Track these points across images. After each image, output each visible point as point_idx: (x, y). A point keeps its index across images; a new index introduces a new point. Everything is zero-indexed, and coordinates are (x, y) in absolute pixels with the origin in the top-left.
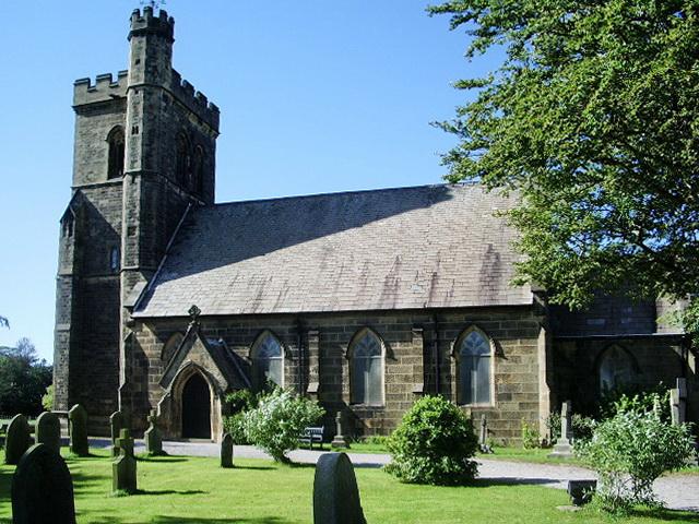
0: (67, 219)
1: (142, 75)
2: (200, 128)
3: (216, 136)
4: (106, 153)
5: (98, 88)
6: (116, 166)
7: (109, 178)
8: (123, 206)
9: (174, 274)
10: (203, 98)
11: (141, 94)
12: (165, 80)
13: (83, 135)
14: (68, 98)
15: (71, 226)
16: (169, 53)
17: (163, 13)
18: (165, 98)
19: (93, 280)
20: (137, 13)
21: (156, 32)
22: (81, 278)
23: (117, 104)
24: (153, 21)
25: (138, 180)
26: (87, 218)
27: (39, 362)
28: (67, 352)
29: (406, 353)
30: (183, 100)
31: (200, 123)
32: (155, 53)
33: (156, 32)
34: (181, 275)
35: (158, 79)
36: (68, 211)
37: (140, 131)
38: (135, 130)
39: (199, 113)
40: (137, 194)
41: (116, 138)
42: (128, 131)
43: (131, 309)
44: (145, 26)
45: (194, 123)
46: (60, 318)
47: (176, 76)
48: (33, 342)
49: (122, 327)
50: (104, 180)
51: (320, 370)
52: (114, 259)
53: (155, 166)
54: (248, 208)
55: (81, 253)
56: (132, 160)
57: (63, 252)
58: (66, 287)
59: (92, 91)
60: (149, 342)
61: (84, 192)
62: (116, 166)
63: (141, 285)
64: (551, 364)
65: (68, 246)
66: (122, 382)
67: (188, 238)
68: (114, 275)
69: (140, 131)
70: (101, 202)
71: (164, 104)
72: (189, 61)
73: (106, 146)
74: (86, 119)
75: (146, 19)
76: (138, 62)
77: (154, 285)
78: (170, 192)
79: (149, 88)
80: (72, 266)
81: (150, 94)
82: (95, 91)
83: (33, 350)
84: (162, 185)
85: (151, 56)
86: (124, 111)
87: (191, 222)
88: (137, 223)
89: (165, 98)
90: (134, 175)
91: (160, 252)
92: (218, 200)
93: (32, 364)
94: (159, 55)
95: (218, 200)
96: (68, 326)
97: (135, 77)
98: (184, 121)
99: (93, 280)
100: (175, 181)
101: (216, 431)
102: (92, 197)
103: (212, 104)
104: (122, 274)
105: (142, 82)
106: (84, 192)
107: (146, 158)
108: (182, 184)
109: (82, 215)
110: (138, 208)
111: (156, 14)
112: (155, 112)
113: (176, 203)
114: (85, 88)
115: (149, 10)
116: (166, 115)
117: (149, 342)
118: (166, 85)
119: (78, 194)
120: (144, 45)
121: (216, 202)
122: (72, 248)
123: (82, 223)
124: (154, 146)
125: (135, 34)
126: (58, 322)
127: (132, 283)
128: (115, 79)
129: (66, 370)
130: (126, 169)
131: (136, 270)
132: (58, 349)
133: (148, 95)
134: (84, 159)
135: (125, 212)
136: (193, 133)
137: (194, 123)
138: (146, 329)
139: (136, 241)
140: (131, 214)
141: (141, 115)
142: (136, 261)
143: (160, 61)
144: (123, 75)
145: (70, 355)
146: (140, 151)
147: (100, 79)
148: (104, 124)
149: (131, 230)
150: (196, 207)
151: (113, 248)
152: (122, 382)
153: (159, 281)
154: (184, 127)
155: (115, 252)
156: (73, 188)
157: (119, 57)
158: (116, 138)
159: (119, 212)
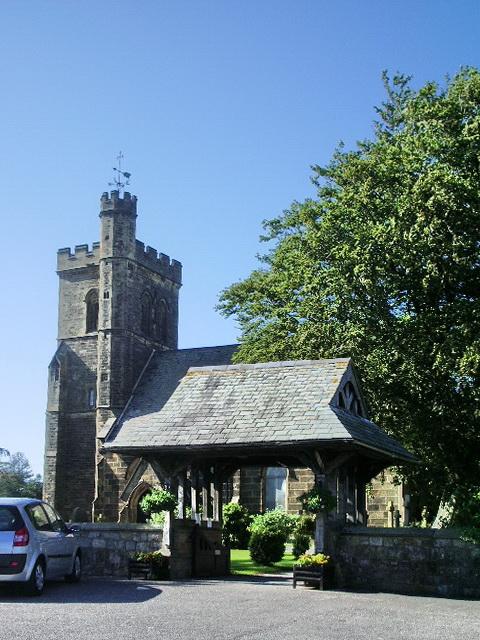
0: (54, 364)
1: (111, 249)
2: (163, 284)
3: (179, 288)
4: (85, 311)
5: (77, 256)
6: (92, 324)
7: (87, 332)
8: (98, 355)
9: (138, 411)
10: (165, 258)
11: (110, 265)
12: (130, 251)
13: (65, 295)
14: (52, 264)
15: (57, 371)
16: (132, 228)
17: (127, 194)
18: (131, 267)
19: (74, 416)
20: (105, 195)
21: (121, 210)
22: (65, 413)
23: (91, 271)
24: (119, 203)
25: (109, 336)
26: (70, 365)
27: (33, 478)
28: (53, 473)
29: (303, 473)
30: (146, 265)
31: (163, 279)
32: (121, 229)
33: (121, 210)
34: (144, 412)
35: (124, 251)
36: (55, 358)
37: (111, 295)
38: (106, 295)
39: (161, 272)
40: (109, 347)
41: (92, 296)
42: (101, 295)
43: (103, 440)
44: (112, 208)
45: (157, 280)
46: (48, 449)
47: (140, 244)
48: (27, 456)
49: (97, 453)
50: (82, 333)
51: (241, 487)
52: (92, 398)
53: (123, 323)
54: (199, 354)
55: (66, 394)
56: (105, 320)
57: (52, 389)
58: (52, 421)
59: (72, 258)
60: (117, 466)
61: (68, 343)
62: (92, 324)
63: (111, 421)
64: (306, 444)
65: (55, 388)
66: (96, 496)
67: (150, 380)
68: (92, 411)
69: (111, 295)
70: (81, 352)
71: (129, 272)
72: (149, 232)
73: (84, 305)
74: (68, 283)
75: (112, 201)
76: (107, 238)
77: (122, 420)
78: (136, 344)
79: (115, 261)
80: (58, 405)
81: (118, 265)
82: (75, 259)
83: (27, 465)
84: (129, 339)
85: (118, 232)
86: (98, 277)
87: (154, 366)
88: (108, 371)
89: (131, 267)
90: (106, 332)
91: (127, 394)
92: (181, 346)
93: (27, 480)
94: (124, 231)
95: (181, 346)
96: (54, 453)
97: (106, 251)
98: (148, 281)
99: (74, 416)
100: (140, 332)
101: (104, 354)
102: (75, 347)
103: (174, 261)
104: (98, 411)
105: (111, 255)
106: (68, 343)
107: (116, 317)
108: (146, 332)
109: (66, 363)
110: (109, 359)
111: (121, 196)
112: (122, 280)
113: (141, 351)
114: (66, 257)
115: (116, 193)
116: (131, 280)
117: (117, 466)
118: (131, 256)
119: (62, 343)
120: (111, 224)
121: (180, 348)
122: (58, 390)
123: (67, 370)
124: (122, 307)
125: (104, 214)
126: (47, 450)
127: (105, 419)
128: (90, 249)
129: (53, 488)
130: (100, 327)
131: (107, 409)
132: (47, 471)
133: (116, 265)
134: (66, 315)
135: (100, 361)
136: (156, 290)
137: (157, 280)
138: (115, 456)
139: (108, 385)
140: (104, 364)
141: (110, 283)
142: (108, 401)
143: (125, 238)
144: (96, 246)
145: (56, 477)
146: (110, 312)
147: (78, 249)
148: (83, 288)
149: (104, 376)
150: (160, 353)
151: (91, 389)
152: (96, 496)
153: (127, 417)
154: (148, 287)
155: (92, 393)
156: (59, 340)
157: (91, 230)
158: (92, 296)
159: (95, 360)
